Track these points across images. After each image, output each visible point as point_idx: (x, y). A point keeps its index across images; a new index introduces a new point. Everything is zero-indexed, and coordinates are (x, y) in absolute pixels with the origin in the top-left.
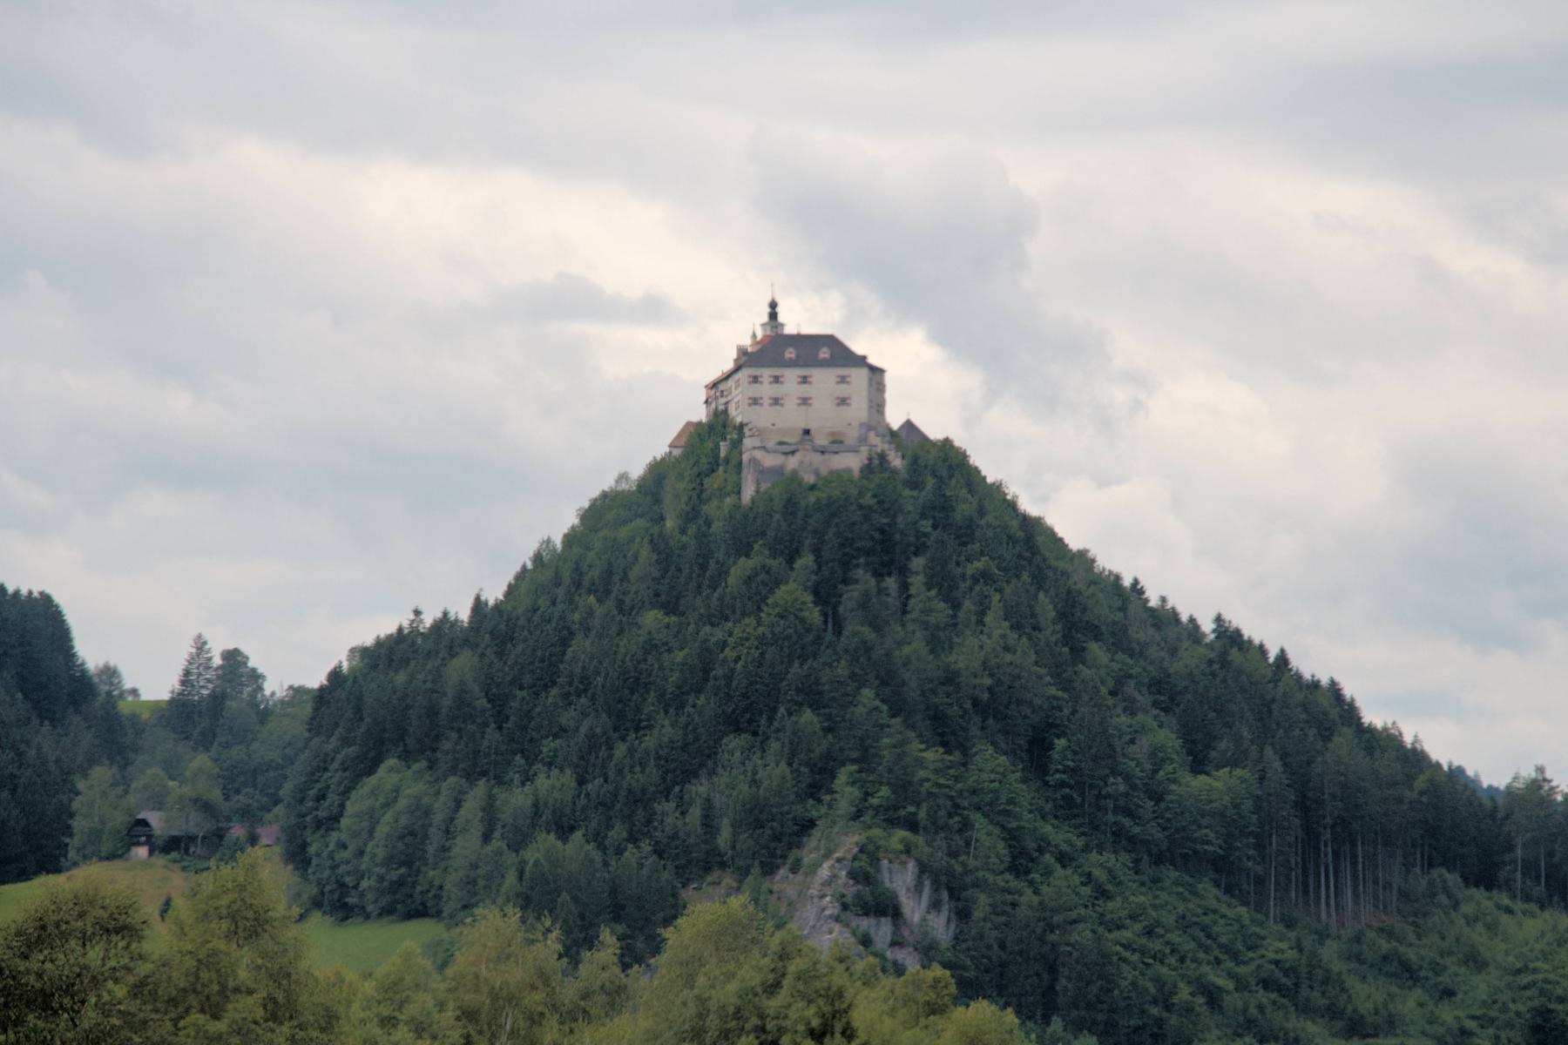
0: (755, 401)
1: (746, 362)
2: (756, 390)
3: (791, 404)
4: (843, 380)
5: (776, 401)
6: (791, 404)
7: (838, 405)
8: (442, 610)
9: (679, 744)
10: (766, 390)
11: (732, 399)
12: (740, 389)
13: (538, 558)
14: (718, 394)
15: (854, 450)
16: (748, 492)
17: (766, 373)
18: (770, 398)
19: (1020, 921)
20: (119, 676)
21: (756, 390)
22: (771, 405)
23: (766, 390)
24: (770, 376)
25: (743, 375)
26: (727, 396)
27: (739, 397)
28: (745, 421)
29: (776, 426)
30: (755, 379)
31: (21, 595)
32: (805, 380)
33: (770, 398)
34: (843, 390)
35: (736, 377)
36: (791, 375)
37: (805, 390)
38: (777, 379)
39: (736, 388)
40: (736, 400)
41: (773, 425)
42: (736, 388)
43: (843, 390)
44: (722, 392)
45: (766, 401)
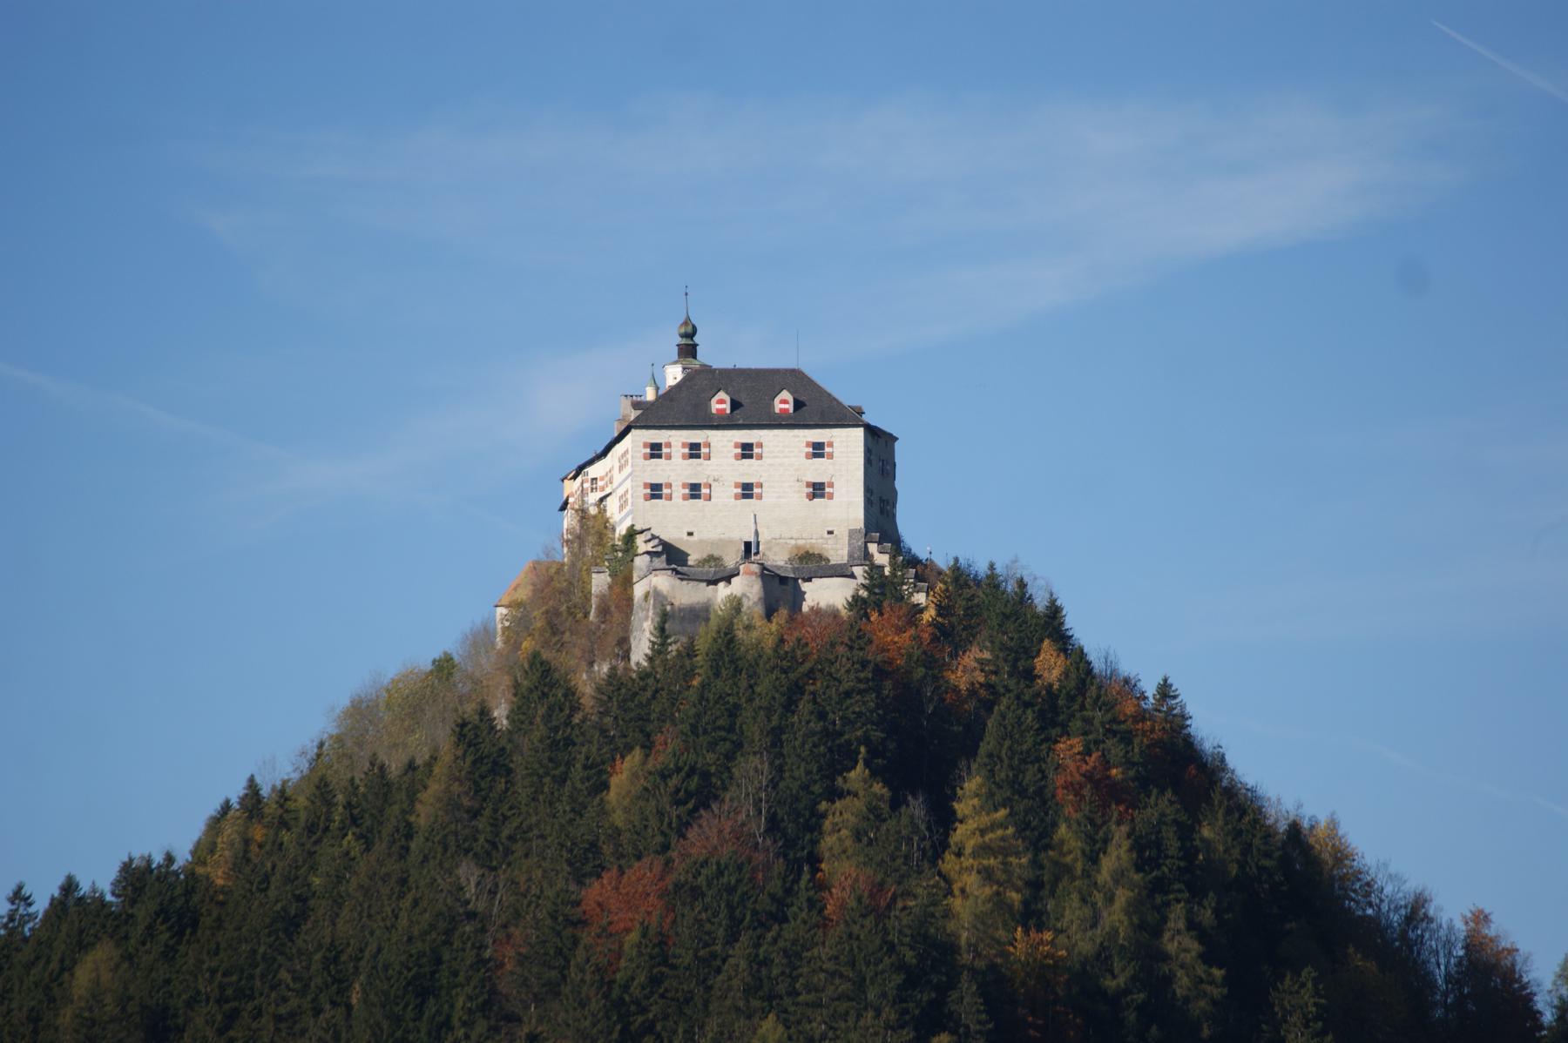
0: (655, 491)
1: (637, 419)
2: (658, 471)
3: (724, 494)
4: (818, 450)
5: (695, 491)
6: (724, 494)
7: (813, 496)
8: (60, 880)
9: (601, 1014)
10: (676, 470)
11: (614, 490)
12: (627, 470)
13: (51, 904)
14: (587, 485)
15: (843, 572)
16: (641, 647)
17: (677, 439)
18: (684, 486)
19: (512, 761)
20: (361, 701)
21: (658, 471)
22: (685, 498)
23: (676, 470)
24: (684, 445)
25: (637, 440)
26: (603, 489)
27: (628, 484)
28: (638, 528)
29: (695, 538)
30: (655, 451)
31: (1032, 606)
32: (747, 451)
33: (684, 486)
34: (818, 470)
35: (619, 449)
36: (723, 442)
37: (749, 470)
38: (694, 451)
39: (621, 468)
40: (620, 491)
41: (690, 534)
42: (621, 468)
43: (818, 470)
44: (594, 480)
45: (679, 492)
